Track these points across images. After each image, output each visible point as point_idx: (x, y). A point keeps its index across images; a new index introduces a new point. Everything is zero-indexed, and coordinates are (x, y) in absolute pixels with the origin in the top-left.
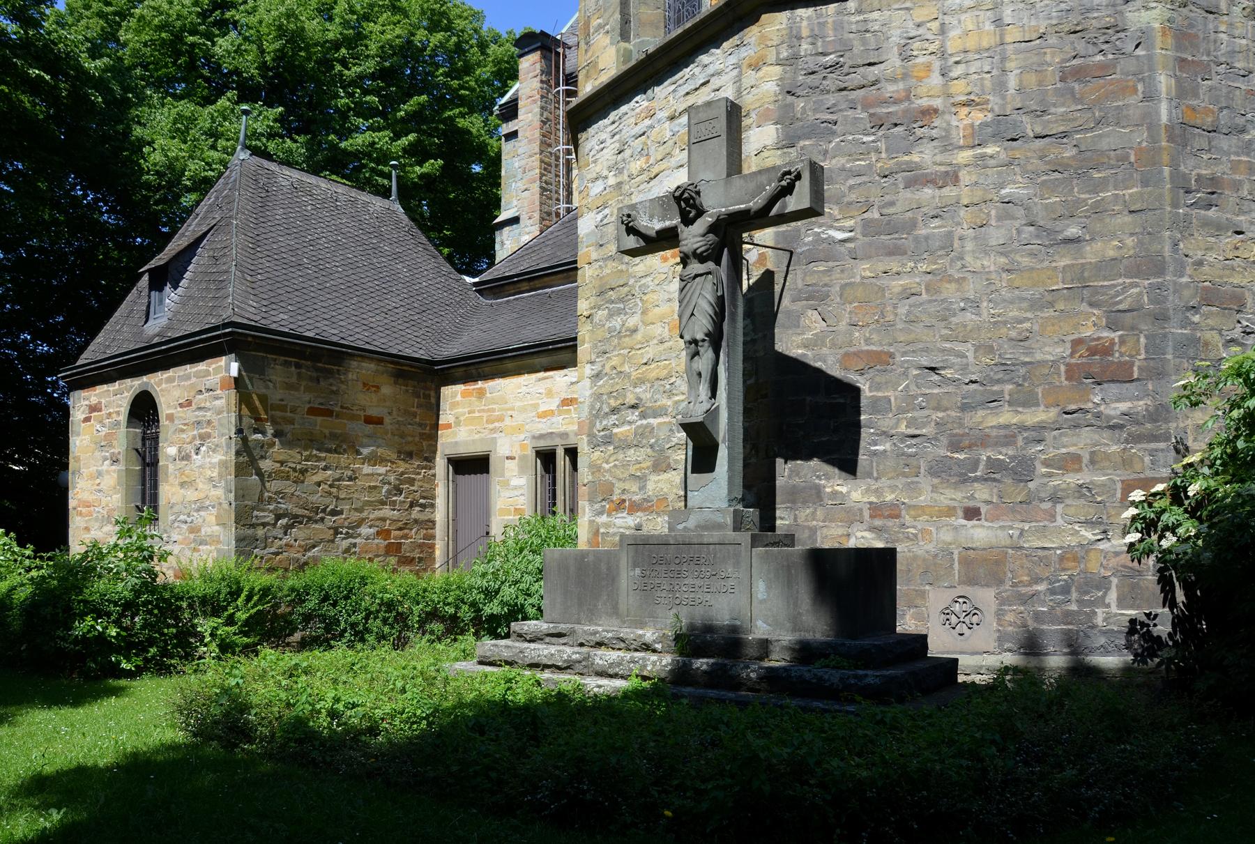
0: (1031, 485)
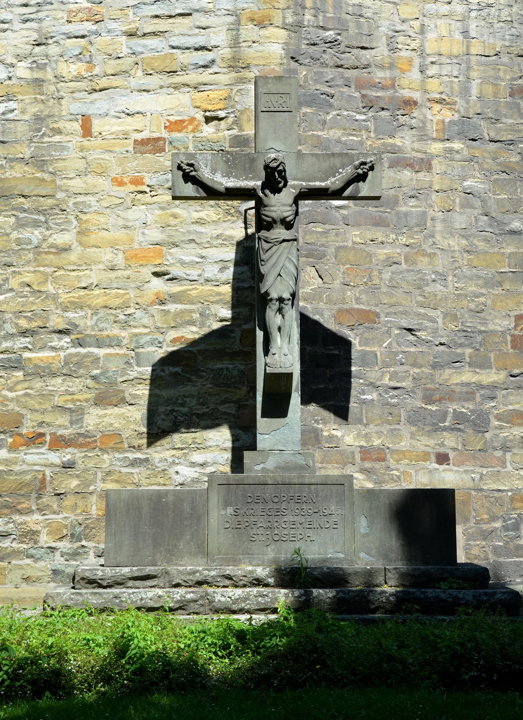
0: (487, 435)
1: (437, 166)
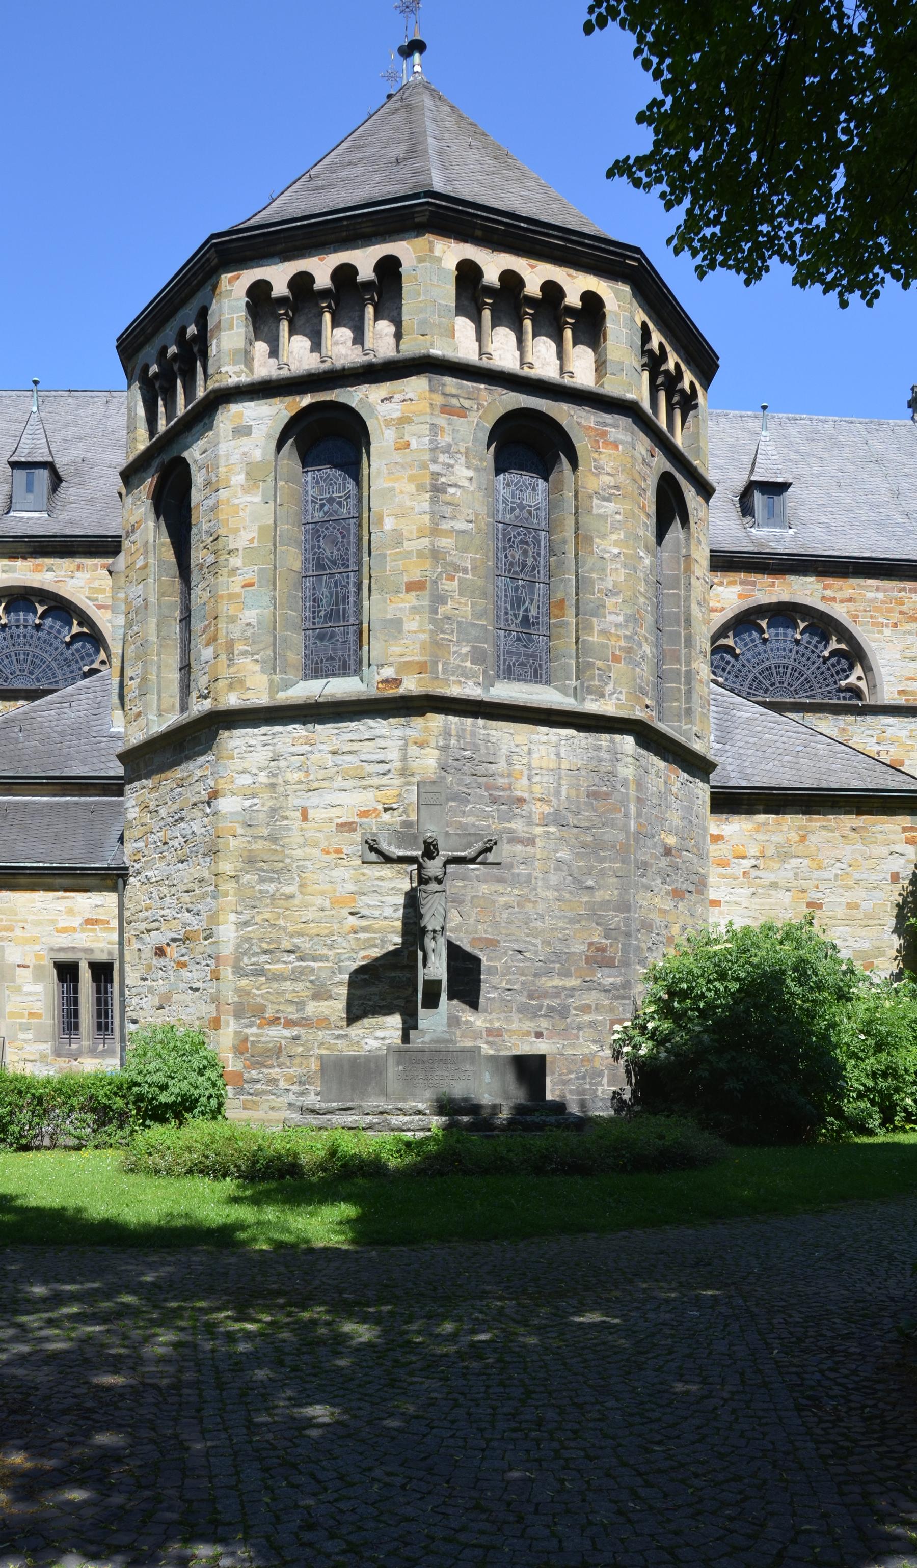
1: (539, 843)
